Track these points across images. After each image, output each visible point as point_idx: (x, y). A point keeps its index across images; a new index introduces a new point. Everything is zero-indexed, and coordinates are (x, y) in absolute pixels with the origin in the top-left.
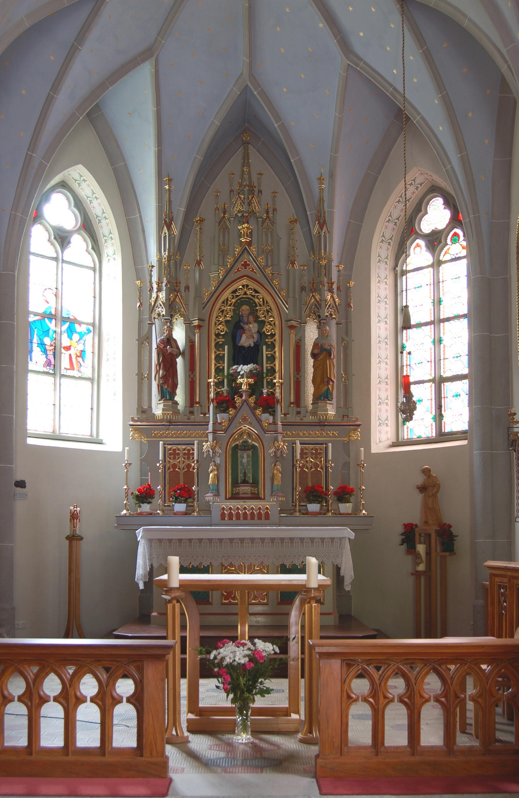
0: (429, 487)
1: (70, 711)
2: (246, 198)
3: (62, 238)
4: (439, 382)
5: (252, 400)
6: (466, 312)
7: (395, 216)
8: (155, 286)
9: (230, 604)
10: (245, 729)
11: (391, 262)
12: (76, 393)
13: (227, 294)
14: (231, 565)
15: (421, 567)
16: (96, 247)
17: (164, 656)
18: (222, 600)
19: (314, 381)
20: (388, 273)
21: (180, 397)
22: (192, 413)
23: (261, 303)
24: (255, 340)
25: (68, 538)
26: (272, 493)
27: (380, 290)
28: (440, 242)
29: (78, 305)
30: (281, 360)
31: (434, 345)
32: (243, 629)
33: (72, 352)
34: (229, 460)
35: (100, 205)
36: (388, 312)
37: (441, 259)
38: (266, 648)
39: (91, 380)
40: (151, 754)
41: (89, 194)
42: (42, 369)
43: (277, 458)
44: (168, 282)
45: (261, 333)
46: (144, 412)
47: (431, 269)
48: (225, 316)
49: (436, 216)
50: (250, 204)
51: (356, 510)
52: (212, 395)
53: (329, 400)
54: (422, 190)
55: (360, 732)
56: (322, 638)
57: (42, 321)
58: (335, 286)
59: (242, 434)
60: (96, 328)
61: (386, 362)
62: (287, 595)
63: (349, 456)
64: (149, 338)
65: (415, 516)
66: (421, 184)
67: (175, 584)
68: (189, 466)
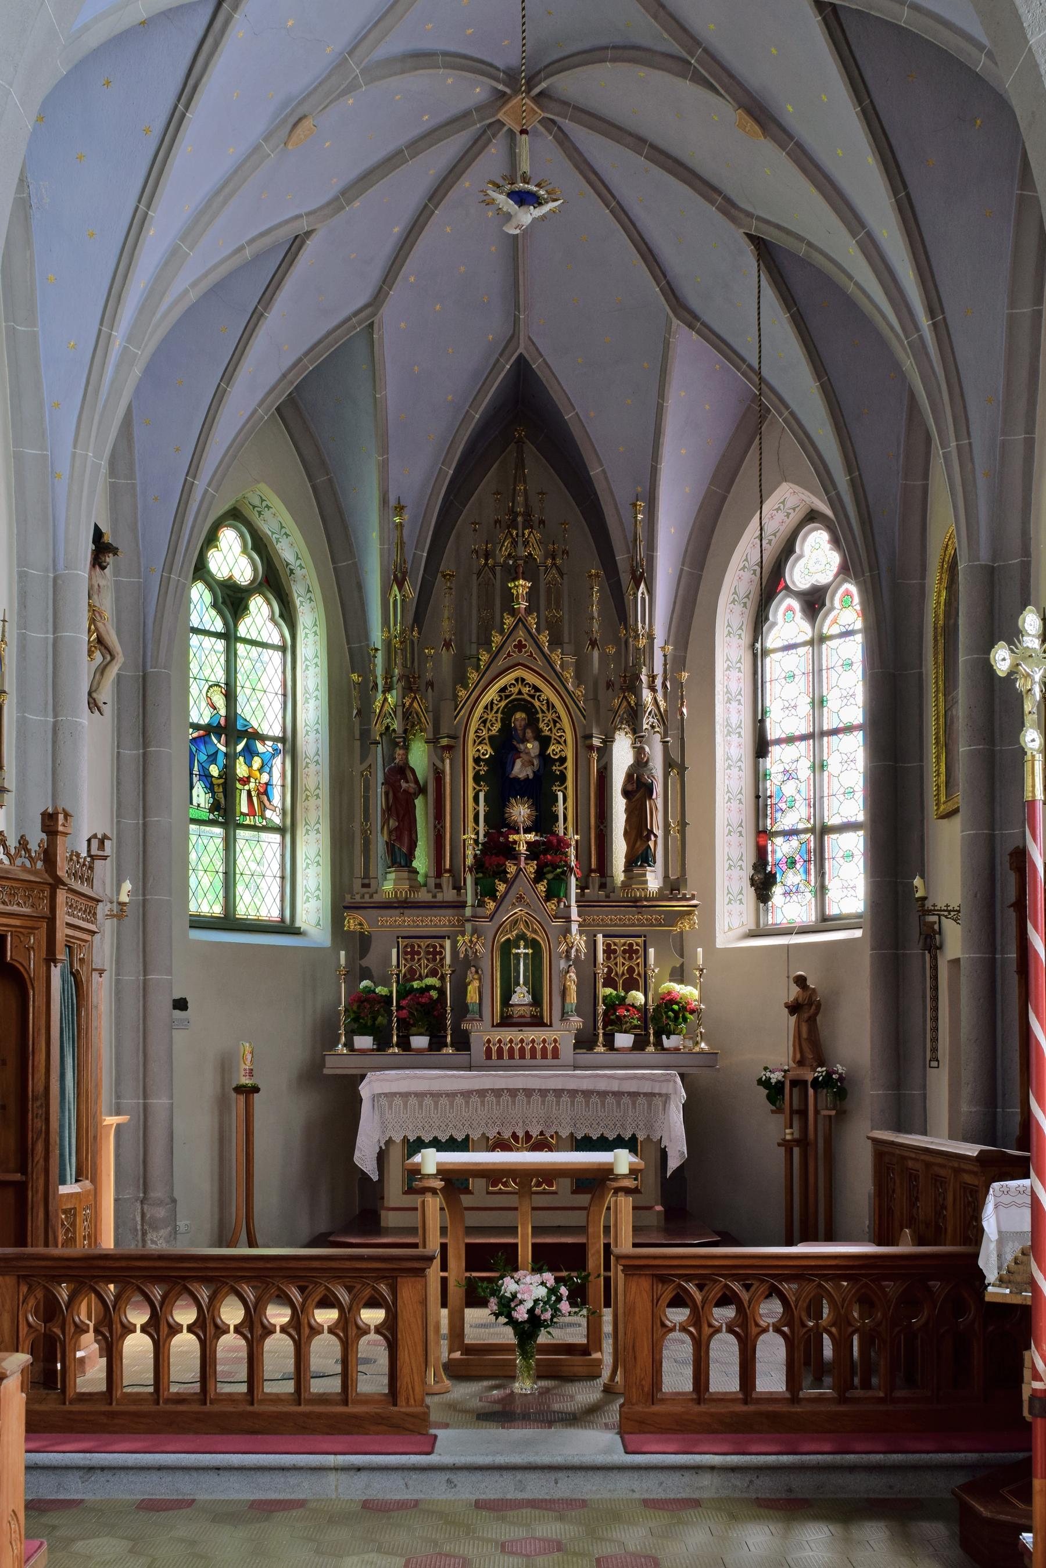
0: (807, 1008)
1: (303, 1346)
2: (520, 534)
3: (232, 600)
4: (823, 831)
11: (746, 637)
16: (288, 615)
17: (424, 1269)
18: (487, 1188)
19: (626, 834)
20: (742, 652)
21: (421, 862)
22: (438, 886)
23: (545, 708)
24: (536, 769)
26: (563, 1016)
28: (823, 605)
31: (814, 772)
36: (742, 717)
37: (825, 631)
40: (408, 1403)
41: (276, 527)
42: (205, 815)
45: (543, 755)
47: (808, 649)
48: (489, 730)
53: (650, 866)
54: (795, 517)
56: (635, 1245)
57: (207, 738)
58: (658, 682)
61: (740, 800)
66: (794, 509)
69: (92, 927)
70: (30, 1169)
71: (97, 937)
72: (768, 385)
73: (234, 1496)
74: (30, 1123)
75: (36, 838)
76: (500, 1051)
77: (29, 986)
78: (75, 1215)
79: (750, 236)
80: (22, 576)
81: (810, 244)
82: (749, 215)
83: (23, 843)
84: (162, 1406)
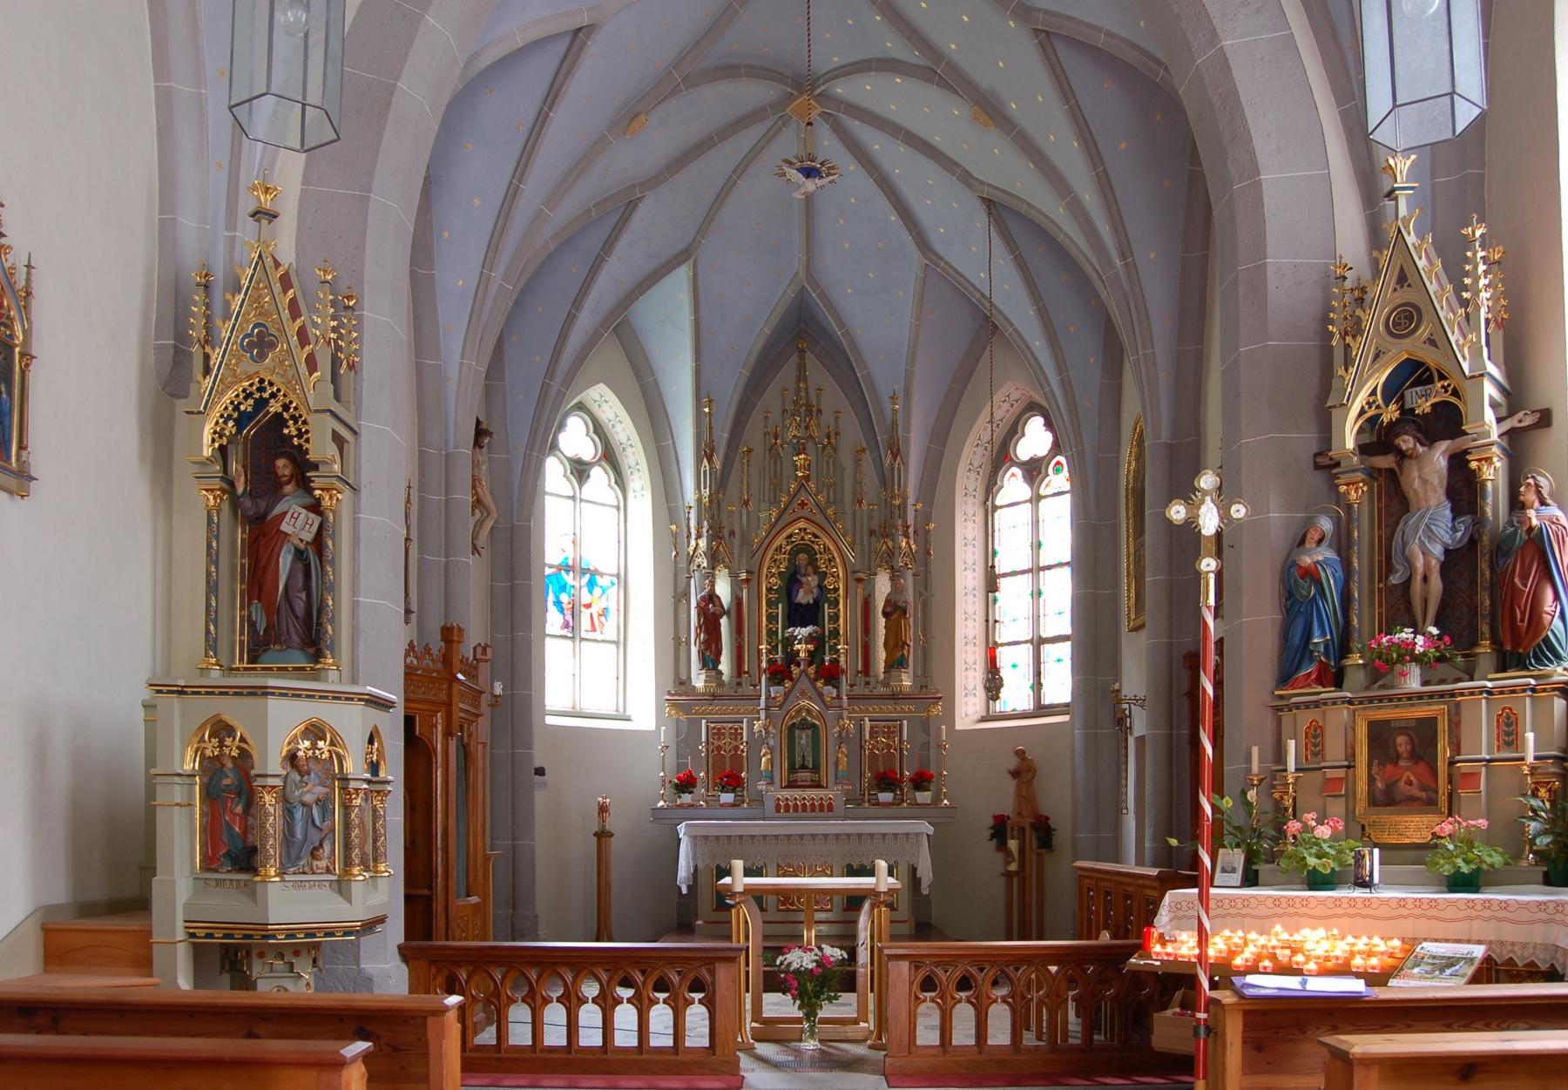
0: (1024, 772)
3: (580, 470)
4: (1038, 642)
5: (812, 670)
6: (1068, 559)
7: (976, 464)
8: (693, 531)
9: (788, 910)
10: (812, 1035)
11: (980, 495)
12: (598, 657)
13: (781, 540)
14: (789, 865)
15: (1013, 867)
16: (621, 482)
21: (725, 666)
22: (739, 684)
25: (596, 834)
27: (966, 530)
29: (600, 555)
30: (846, 614)
32: (810, 935)
33: (594, 610)
34: (785, 743)
35: (624, 430)
38: (835, 953)
39: (617, 643)
41: (612, 417)
43: (842, 739)
44: (710, 527)
45: (821, 587)
46: (682, 683)
49: (1035, 439)
50: (807, 428)
51: (937, 800)
52: (764, 665)
54: (1018, 407)
55: (927, 1035)
58: (911, 530)
59: (799, 711)
60: (622, 579)
62: (854, 901)
63: (928, 734)
64: (687, 595)
65: (1007, 807)
67: (739, 888)
68: (736, 748)
72: (997, 309)
75: (437, 645)
76: (787, 806)
79: (982, 198)
81: (1029, 205)
82: (983, 183)
83: (427, 650)
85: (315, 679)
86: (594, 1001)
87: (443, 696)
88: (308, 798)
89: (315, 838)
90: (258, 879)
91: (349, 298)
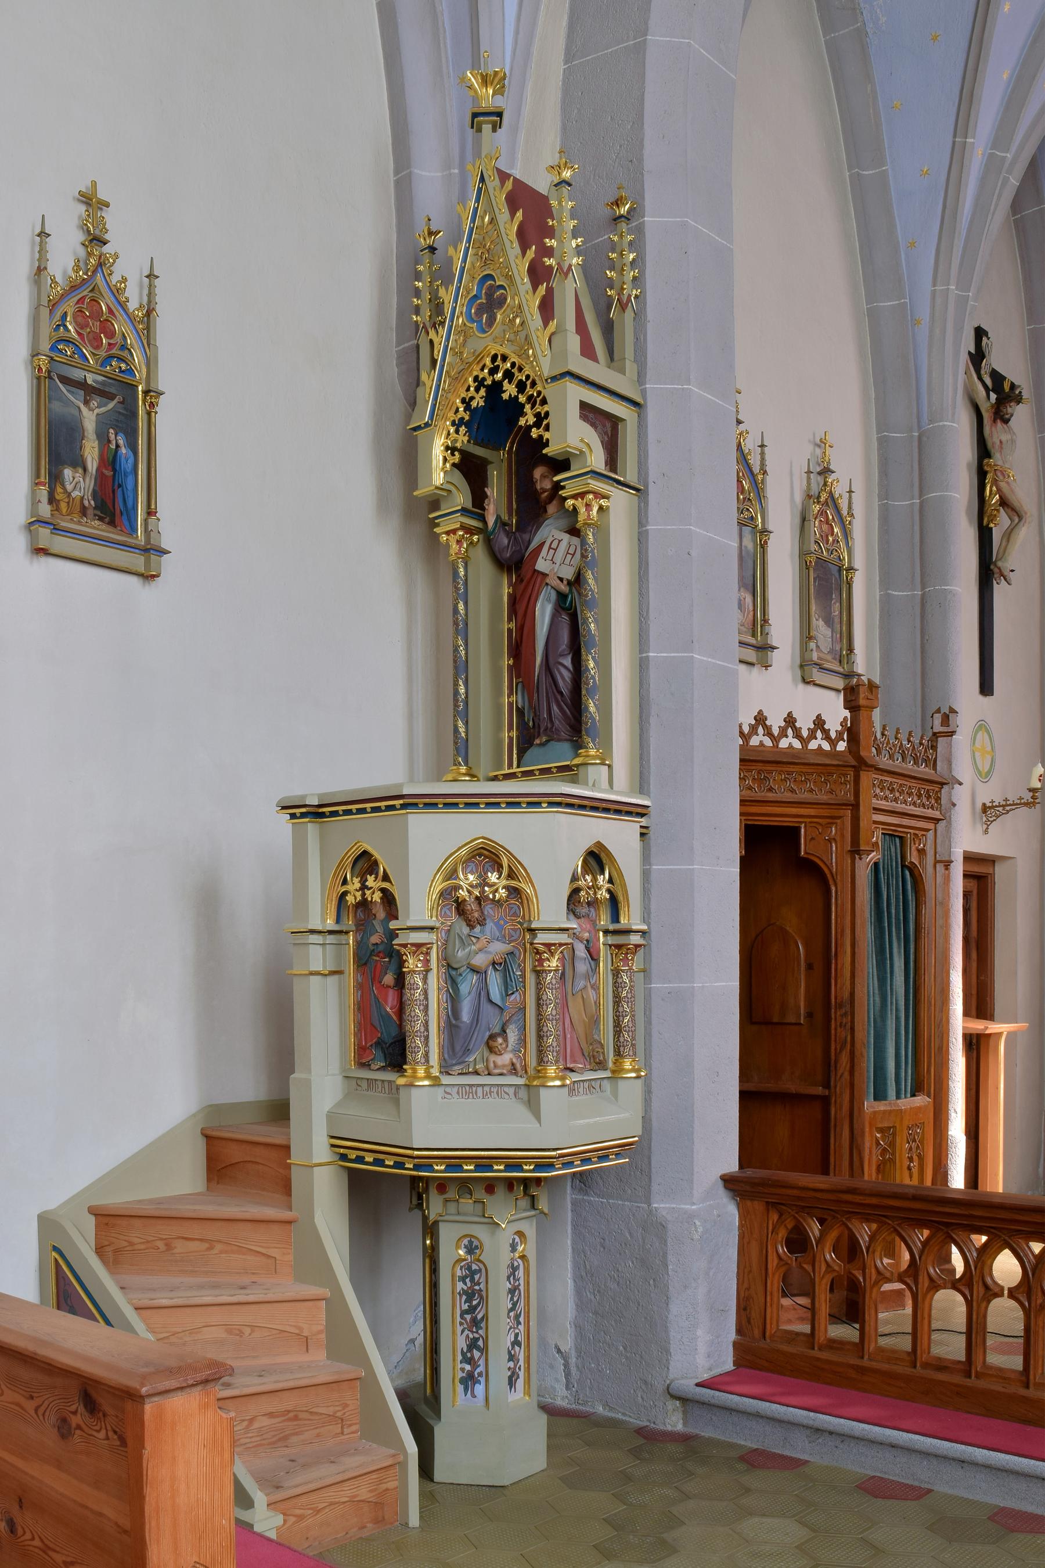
69: (936, 814)
70: (832, 1083)
71: (941, 826)
73: (979, 1497)
74: (833, 1032)
77: (831, 882)
78: (894, 1134)
80: (883, 442)
84: (919, 1370)
85: (574, 780)
86: (1013, 1294)
87: (845, 793)
88: (480, 960)
89: (492, 1020)
90: (401, 1081)
91: (618, 203)
